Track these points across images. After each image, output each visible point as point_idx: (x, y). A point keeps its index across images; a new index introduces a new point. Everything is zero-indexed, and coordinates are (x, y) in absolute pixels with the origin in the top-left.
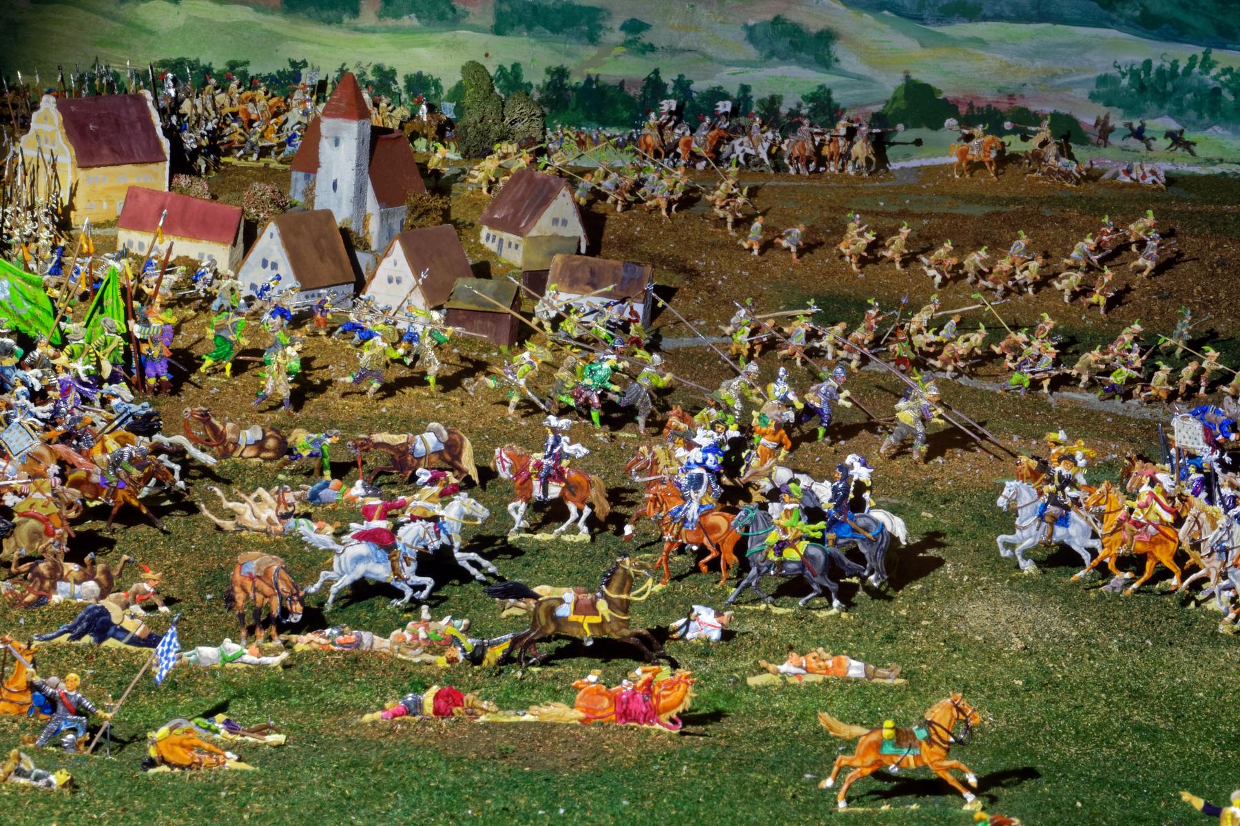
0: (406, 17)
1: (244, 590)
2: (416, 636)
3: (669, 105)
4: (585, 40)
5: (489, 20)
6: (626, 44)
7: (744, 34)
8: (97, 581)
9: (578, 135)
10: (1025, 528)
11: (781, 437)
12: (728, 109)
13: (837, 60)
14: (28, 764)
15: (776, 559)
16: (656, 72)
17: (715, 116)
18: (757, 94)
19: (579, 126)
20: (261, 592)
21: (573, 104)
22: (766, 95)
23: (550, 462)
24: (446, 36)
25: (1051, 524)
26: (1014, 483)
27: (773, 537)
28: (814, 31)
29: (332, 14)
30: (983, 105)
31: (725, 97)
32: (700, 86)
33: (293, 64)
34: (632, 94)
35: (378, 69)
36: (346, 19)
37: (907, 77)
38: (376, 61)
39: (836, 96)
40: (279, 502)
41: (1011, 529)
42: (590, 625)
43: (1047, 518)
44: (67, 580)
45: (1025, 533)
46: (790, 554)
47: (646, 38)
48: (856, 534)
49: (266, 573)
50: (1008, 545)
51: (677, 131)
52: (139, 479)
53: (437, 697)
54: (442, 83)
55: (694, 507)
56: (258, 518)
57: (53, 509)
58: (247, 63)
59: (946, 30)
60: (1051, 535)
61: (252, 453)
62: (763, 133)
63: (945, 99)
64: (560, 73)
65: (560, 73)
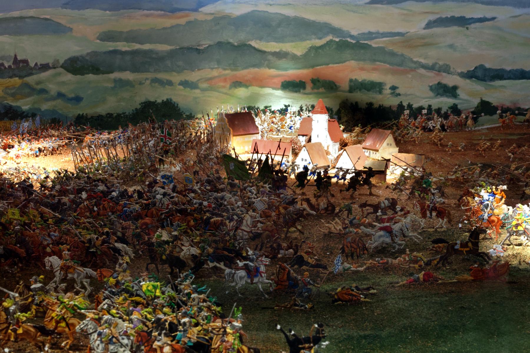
1: (348, 247)
2: (405, 259)
3: (407, 112)
6: (392, 93)
7: (429, 88)
8: (293, 249)
12: (426, 112)
14: (299, 302)
16: (401, 102)
17: (422, 115)
20: (353, 248)
22: (437, 108)
27: (514, 223)
29: (296, 89)
30: (505, 107)
31: (424, 109)
32: (415, 106)
33: (285, 106)
36: (302, 91)
37: (481, 99)
39: (459, 107)
40: (343, 224)
42: (466, 251)
44: (283, 250)
47: (398, 91)
49: (355, 241)
52: (296, 219)
53: (424, 275)
55: (486, 215)
56: (336, 229)
57: (274, 227)
58: (270, 106)
59: (492, 83)
61: (324, 212)
63: (494, 106)
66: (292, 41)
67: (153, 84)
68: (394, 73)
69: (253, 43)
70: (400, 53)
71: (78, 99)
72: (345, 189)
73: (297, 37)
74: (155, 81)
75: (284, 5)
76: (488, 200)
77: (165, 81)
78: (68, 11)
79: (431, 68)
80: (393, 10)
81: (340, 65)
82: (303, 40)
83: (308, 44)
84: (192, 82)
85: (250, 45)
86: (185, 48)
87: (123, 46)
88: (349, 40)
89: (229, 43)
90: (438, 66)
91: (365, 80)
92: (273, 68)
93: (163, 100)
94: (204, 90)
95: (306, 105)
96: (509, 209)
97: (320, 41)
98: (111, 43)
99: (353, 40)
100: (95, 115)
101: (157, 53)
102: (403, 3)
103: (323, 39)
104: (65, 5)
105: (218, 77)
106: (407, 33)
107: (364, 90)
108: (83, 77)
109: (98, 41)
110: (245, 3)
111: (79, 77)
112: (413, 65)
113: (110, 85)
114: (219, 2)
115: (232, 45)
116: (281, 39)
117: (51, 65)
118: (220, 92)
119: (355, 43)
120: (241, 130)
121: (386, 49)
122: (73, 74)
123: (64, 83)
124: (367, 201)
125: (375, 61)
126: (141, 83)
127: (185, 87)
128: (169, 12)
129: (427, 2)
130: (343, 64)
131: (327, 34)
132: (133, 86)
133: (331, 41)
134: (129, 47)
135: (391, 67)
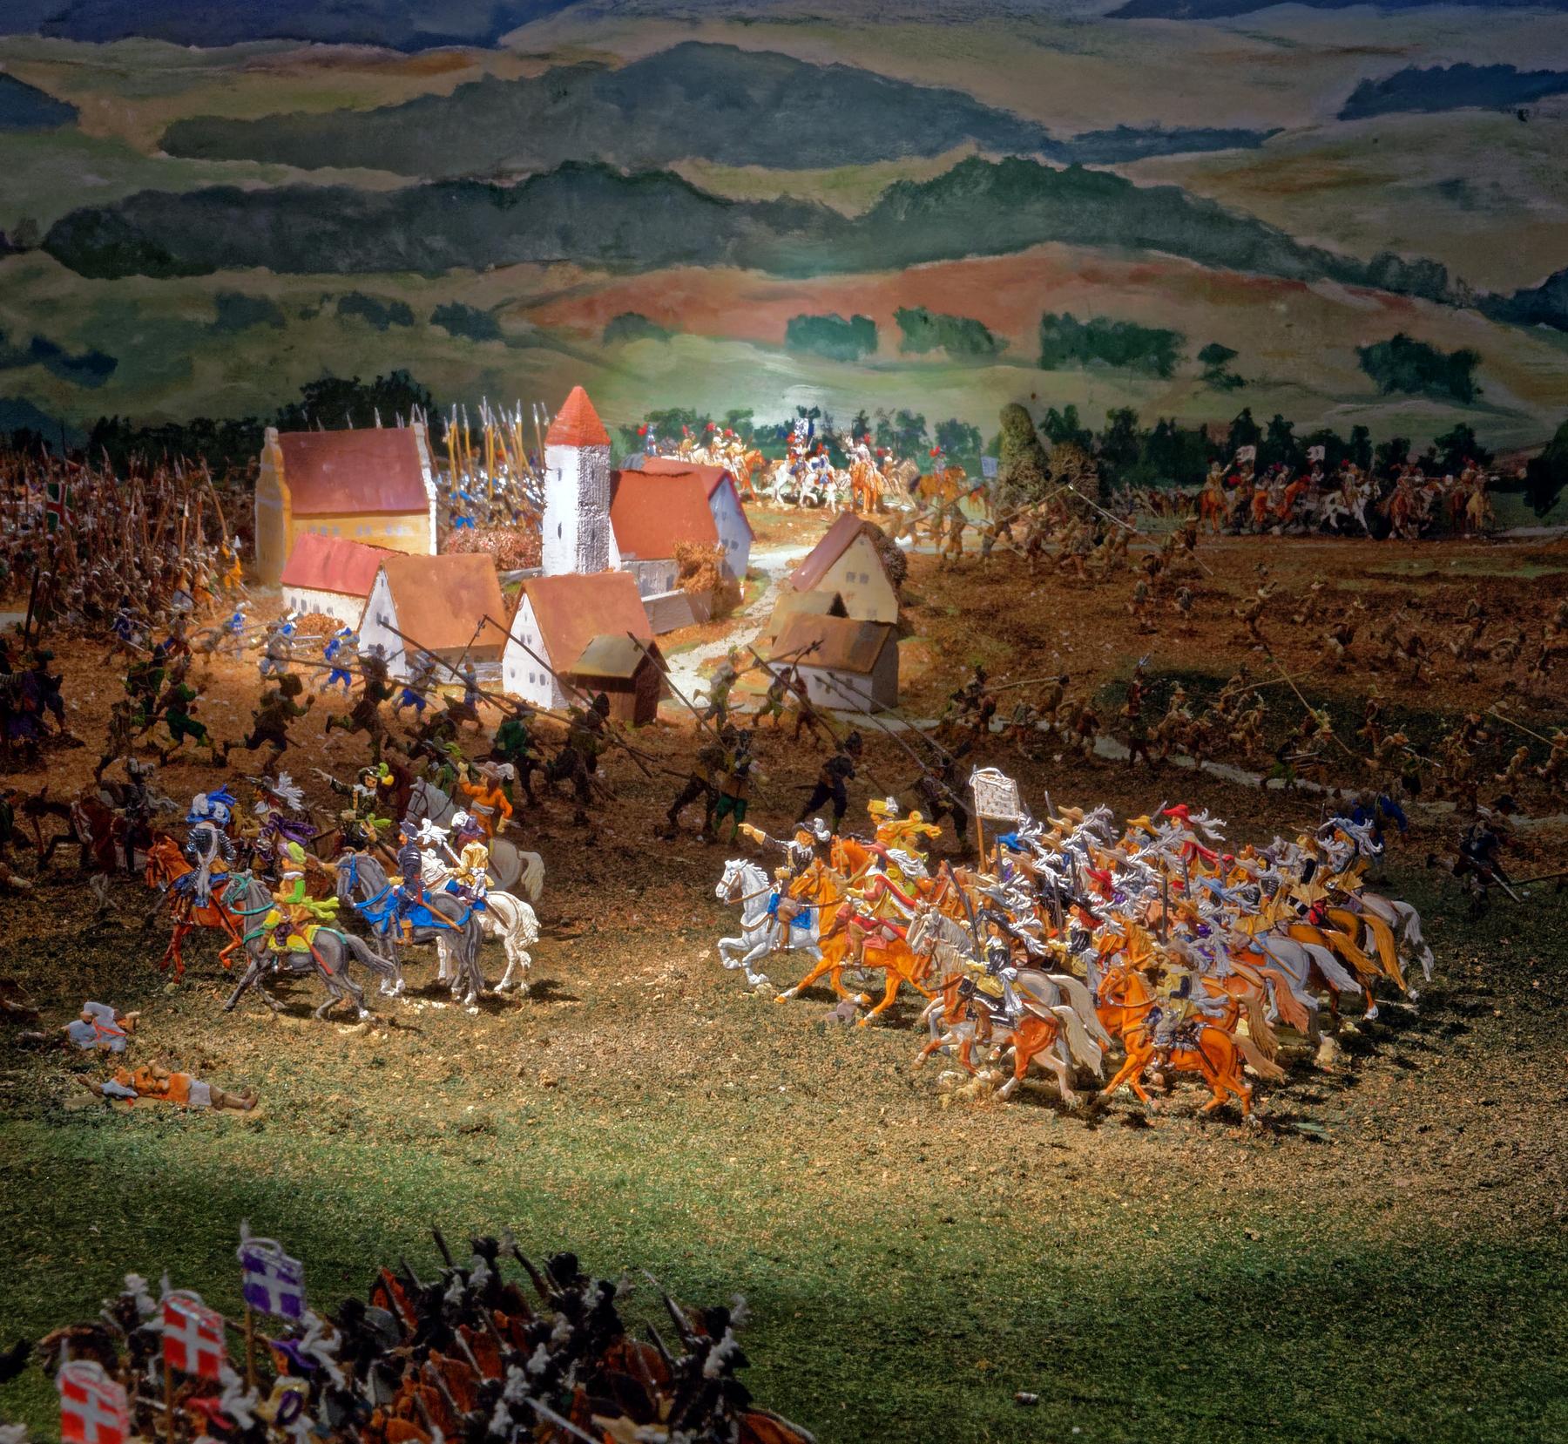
0: (933, 351)
4: (1156, 374)
5: (1035, 351)
6: (1208, 377)
7: (1358, 359)
9: (1151, 497)
10: (753, 929)
11: (498, 801)
12: (1322, 456)
13: (1479, 391)
15: (278, 949)
16: (1247, 412)
18: (1375, 439)
19: (1152, 484)
21: (1143, 456)
23: (134, 822)
24: (984, 372)
25: (787, 924)
26: (737, 863)
28: (1447, 352)
29: (844, 348)
34: (1217, 441)
35: (904, 417)
36: (862, 356)
38: (900, 407)
39: (1479, 438)
41: (735, 931)
43: (780, 916)
45: (753, 936)
46: (296, 943)
47: (1232, 368)
48: (438, 922)
50: (732, 952)
51: (1258, 486)
54: (981, 433)
55: (204, 876)
60: (787, 941)
62: (1358, 485)
64: (1126, 418)
65: (1126, 418)
66: (825, 164)
67: (345, 316)
68: (1218, 292)
69: (684, 169)
70: (1240, 215)
71: (98, 365)
72: (242, 741)
73: (844, 149)
74: (354, 303)
75: (796, 22)
76: (208, 817)
77: (387, 307)
78: (63, 46)
79: (1365, 278)
80: (1173, 39)
81: (1006, 256)
82: (864, 157)
83: (882, 174)
84: (479, 314)
85: (674, 179)
86: (452, 184)
87: (249, 176)
88: (1040, 158)
89: (602, 167)
90: (1394, 268)
91: (1103, 321)
92: (756, 266)
93: (380, 378)
94: (518, 343)
95: (879, 412)
96: (525, 864)
97: (929, 162)
98: (206, 163)
99: (1058, 158)
100: (153, 425)
101: (357, 200)
102: (1238, 18)
103: (942, 157)
104: (58, 24)
105: (570, 293)
106: (1272, 133)
107: (1098, 360)
108: (115, 283)
109: (163, 155)
110: (655, 14)
111: (100, 285)
112: (1294, 265)
113: (206, 316)
114: (569, 11)
115: (613, 176)
116: (780, 157)
117: (9, 240)
118: (569, 352)
119: (1068, 171)
120: (339, 496)
121: (1186, 197)
122: (84, 274)
123: (50, 307)
124: (45, 790)
125: (1142, 243)
126: (306, 314)
127: (453, 331)
128: (396, 48)
129: (1356, 8)
130: (1019, 255)
131: (951, 138)
132: (280, 323)
133: (973, 162)
134: (264, 177)
135: (1208, 270)
